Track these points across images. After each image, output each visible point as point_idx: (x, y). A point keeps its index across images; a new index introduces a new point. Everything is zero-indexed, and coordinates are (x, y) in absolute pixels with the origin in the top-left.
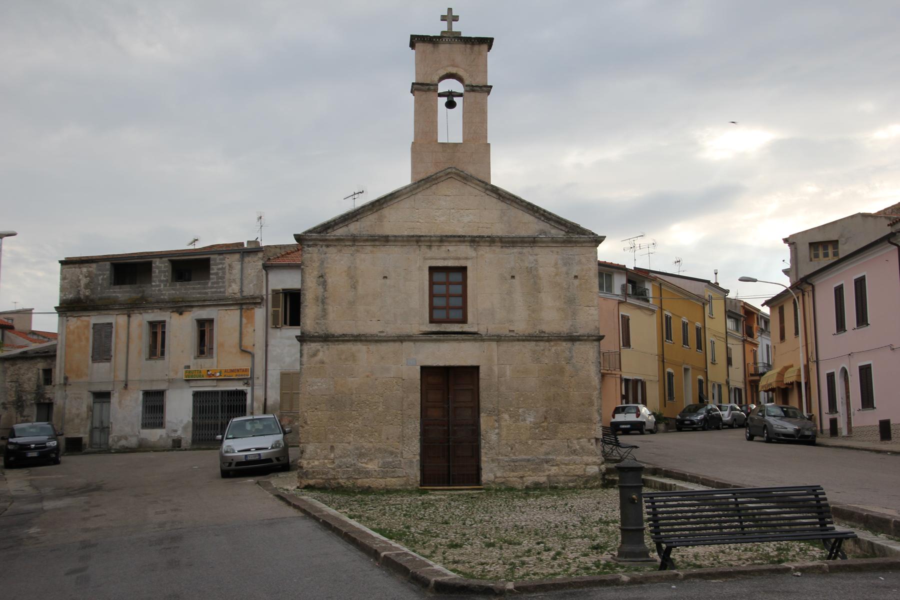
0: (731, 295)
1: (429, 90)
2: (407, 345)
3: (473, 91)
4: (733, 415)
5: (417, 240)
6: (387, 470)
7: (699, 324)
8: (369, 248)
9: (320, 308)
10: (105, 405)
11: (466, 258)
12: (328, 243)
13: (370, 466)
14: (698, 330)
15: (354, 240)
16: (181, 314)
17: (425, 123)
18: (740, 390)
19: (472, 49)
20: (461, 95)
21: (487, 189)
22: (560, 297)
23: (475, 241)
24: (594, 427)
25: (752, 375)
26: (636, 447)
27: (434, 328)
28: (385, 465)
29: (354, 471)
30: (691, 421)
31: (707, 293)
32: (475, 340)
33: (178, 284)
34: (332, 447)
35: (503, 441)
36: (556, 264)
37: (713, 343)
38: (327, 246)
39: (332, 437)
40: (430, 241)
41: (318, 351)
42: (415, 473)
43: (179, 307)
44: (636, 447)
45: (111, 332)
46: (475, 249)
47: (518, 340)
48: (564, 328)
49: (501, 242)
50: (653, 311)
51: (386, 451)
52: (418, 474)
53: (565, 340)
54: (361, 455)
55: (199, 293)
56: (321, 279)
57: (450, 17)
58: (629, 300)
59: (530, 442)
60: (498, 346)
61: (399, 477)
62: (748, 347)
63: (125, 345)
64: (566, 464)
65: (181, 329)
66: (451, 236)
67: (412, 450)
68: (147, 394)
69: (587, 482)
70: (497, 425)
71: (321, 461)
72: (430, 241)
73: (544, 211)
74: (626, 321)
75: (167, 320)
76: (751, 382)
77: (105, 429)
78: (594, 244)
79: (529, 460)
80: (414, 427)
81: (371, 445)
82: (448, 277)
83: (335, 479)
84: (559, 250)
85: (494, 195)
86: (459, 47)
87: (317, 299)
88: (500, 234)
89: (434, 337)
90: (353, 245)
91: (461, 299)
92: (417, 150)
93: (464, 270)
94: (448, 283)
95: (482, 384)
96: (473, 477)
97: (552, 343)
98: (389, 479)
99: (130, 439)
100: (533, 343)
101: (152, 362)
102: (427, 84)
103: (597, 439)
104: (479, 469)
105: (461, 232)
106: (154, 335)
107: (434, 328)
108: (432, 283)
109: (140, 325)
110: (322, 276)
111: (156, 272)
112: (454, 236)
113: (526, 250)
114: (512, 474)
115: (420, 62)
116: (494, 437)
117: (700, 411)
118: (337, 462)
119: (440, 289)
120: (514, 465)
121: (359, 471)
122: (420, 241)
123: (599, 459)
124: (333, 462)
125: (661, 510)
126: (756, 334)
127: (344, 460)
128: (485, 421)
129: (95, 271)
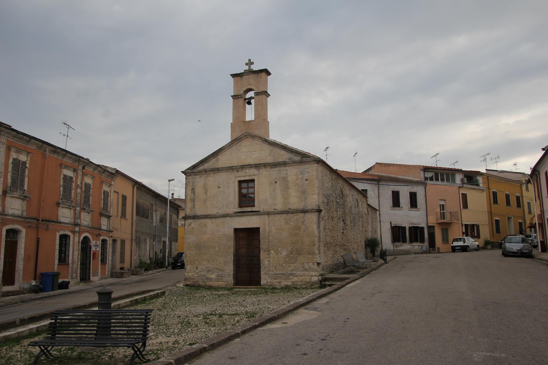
1: (238, 98)
3: (258, 95)
6: (220, 278)
11: (254, 175)
14: (518, 198)
15: (205, 171)
17: (239, 114)
19: (257, 76)
23: (257, 166)
32: (257, 215)
38: (196, 175)
42: (230, 280)
46: (258, 171)
47: (278, 214)
48: (300, 206)
50: (483, 190)
53: (301, 212)
54: (209, 271)
57: (250, 63)
58: (465, 186)
67: (230, 269)
69: (312, 285)
74: (464, 196)
79: (283, 274)
80: (231, 258)
82: (248, 185)
86: (252, 76)
87: (191, 200)
89: (239, 214)
95: (261, 236)
100: (285, 215)
110: (193, 189)
113: (281, 169)
115: (236, 85)
116: (266, 262)
119: (251, 190)
125: (113, 321)
127: (201, 273)
128: (263, 255)
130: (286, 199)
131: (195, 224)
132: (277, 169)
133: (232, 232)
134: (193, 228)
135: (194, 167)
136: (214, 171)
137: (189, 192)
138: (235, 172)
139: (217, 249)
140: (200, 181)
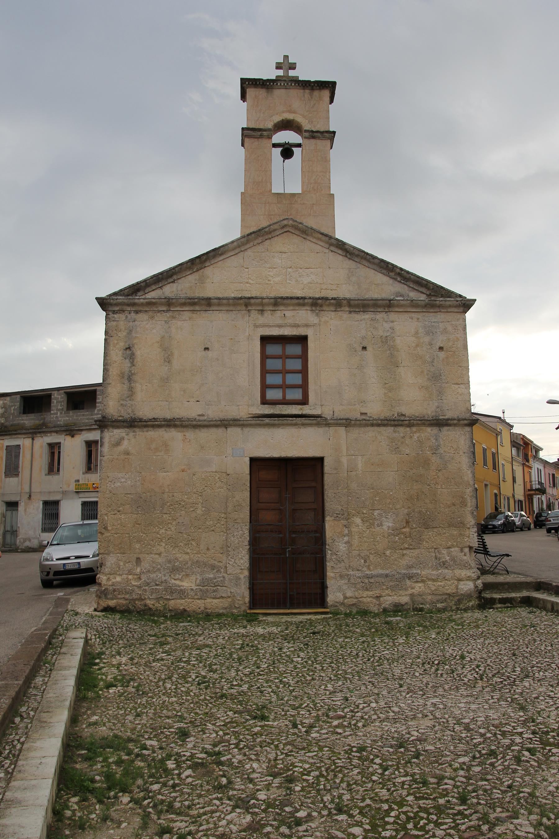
0: (514, 430)
1: (261, 136)
2: (233, 431)
3: (313, 137)
4: (523, 520)
5: (245, 303)
6: (207, 588)
7: (494, 450)
8: (187, 315)
9: (126, 387)
10: (14, 512)
11: (307, 326)
12: (138, 308)
13: (186, 584)
14: (493, 454)
15: (169, 303)
16: (73, 436)
18: (521, 502)
19: (311, 95)
20: (299, 145)
21: (331, 245)
22: (422, 372)
23: (316, 304)
24: (467, 532)
25: (529, 490)
26: (508, 555)
27: (267, 410)
28: (204, 583)
29: (166, 590)
30: (493, 525)
31: (499, 427)
32: (318, 425)
33: (71, 413)
34: (138, 559)
35: (355, 555)
36: (417, 333)
37: (503, 465)
38: (137, 312)
39: (137, 546)
40: (262, 305)
41: (123, 438)
42: (242, 593)
43: (71, 431)
44: (508, 555)
45: (19, 453)
46: (317, 315)
47: (372, 425)
48: (428, 410)
49: (350, 305)
51: (205, 564)
52: (247, 593)
54: (174, 570)
55: (88, 419)
56: (128, 352)
57: (286, 64)
59: (388, 553)
60: (347, 432)
61: (222, 597)
62: (526, 469)
63: (30, 463)
64: (434, 580)
65: (73, 449)
66: (287, 298)
68: (46, 503)
69: (459, 601)
70: (346, 531)
71: (125, 576)
72: (262, 305)
73: (401, 269)
75: (62, 442)
76: (529, 495)
77: (14, 532)
78: (461, 309)
79: (387, 576)
80: (241, 535)
81: (187, 557)
82: (284, 350)
83: (141, 599)
84: (419, 316)
85: (340, 252)
86: (296, 93)
87: (122, 375)
88: (348, 296)
89: (267, 420)
90: (167, 311)
91: (300, 376)
92: (247, 202)
93: (303, 340)
94: (284, 357)
95: (327, 479)
96: (317, 598)
97: (414, 429)
98: (209, 600)
99: (32, 541)
100: (391, 429)
101: (50, 477)
102: (260, 130)
103: (470, 548)
104: (323, 587)
105: (299, 294)
106: (52, 454)
107: (267, 410)
108: (264, 357)
109: (42, 447)
110: (129, 348)
111: (54, 402)
112: (292, 298)
113: (379, 316)
114: (366, 593)
117: (498, 517)
118: (144, 578)
120: (368, 583)
121: (172, 590)
122: (250, 304)
123: (473, 573)
124: (140, 578)
126: (531, 460)
128: (331, 527)
129: (8, 403)
130: (390, 390)
131: (132, 441)
132: (367, 316)
134: (127, 453)
135: (136, 289)
136: (194, 304)
137: (117, 355)
138: (254, 314)
139: (199, 512)
140: (149, 330)
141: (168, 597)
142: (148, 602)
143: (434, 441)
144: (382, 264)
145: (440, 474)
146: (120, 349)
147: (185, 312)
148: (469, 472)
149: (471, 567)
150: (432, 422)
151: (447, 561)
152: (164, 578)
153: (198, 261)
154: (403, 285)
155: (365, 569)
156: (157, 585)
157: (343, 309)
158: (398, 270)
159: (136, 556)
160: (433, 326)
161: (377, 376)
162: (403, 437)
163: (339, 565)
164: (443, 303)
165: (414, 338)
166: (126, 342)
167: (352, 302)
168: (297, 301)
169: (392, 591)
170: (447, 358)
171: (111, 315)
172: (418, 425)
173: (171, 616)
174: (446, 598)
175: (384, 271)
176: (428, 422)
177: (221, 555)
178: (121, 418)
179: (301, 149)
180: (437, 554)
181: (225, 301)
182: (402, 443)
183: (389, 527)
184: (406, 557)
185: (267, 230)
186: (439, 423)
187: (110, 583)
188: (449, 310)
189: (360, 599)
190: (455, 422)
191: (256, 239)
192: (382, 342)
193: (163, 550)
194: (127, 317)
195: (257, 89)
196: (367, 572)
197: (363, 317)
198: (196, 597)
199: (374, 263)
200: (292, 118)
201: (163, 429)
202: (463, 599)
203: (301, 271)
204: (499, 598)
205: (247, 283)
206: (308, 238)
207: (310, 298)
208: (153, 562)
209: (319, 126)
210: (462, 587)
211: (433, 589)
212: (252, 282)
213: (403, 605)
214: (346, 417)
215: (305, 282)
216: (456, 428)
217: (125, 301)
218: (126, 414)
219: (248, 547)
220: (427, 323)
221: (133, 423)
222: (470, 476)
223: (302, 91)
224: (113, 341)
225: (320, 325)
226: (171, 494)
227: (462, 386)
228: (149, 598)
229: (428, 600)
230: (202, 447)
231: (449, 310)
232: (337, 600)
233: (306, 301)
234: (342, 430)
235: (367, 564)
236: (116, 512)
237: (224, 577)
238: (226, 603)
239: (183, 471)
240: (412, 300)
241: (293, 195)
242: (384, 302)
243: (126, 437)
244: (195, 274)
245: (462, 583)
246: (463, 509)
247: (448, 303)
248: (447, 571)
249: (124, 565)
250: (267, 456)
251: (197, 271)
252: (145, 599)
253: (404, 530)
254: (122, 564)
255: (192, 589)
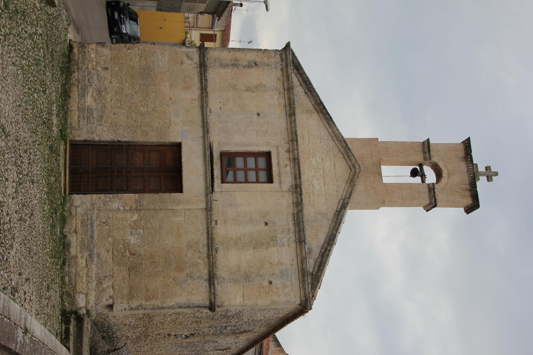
1: (424, 153)
3: (430, 190)
6: (86, 113)
8: (283, 102)
11: (280, 183)
12: (284, 70)
15: (289, 89)
19: (466, 190)
20: (423, 181)
23: (297, 189)
24: (125, 302)
27: (216, 155)
28: (90, 110)
29: (85, 85)
32: (207, 188)
34: (107, 69)
36: (281, 264)
38: (282, 70)
39: (117, 68)
41: (192, 60)
42: (82, 135)
47: (208, 228)
48: (221, 271)
49: (298, 212)
52: (82, 138)
54: (99, 92)
57: (490, 175)
59: (110, 239)
61: (79, 122)
64: (87, 274)
66: (299, 167)
69: (69, 295)
79: (92, 237)
80: (125, 135)
81: (109, 100)
82: (262, 170)
84: (295, 266)
85: (339, 207)
86: (466, 179)
87: (236, 60)
89: (208, 153)
90: (284, 89)
95: (166, 196)
97: (206, 260)
98: (77, 113)
100: (205, 242)
102: (429, 151)
110: (256, 64)
112: (299, 169)
114: (79, 222)
118: (94, 72)
120: (88, 223)
124: (93, 69)
128: (130, 198)
130: (236, 243)
132: (291, 226)
133: (174, 138)
134: (182, 63)
135: (298, 67)
137: (251, 57)
138: (286, 146)
139: (141, 109)
140: (271, 77)
141: (80, 87)
142: (76, 74)
143: (197, 275)
144: (333, 237)
145: (171, 280)
146: (254, 59)
147: (284, 100)
148: (173, 303)
149: (97, 305)
150: (212, 273)
151: (102, 284)
152: (93, 84)
153: (322, 107)
154: (318, 254)
155: (98, 222)
156: (88, 80)
157: (295, 208)
158: (329, 248)
159: (109, 67)
160: (288, 276)
161: (245, 233)
162: (199, 252)
163: (101, 203)
164: (307, 283)
165: (277, 261)
166: (260, 62)
167: (300, 213)
168: (297, 174)
169: (80, 242)
170: (263, 287)
171: (279, 53)
172: (209, 262)
173: (66, 88)
174: (72, 284)
175: (328, 239)
176: (211, 269)
177: (110, 123)
178: (206, 59)
179: (421, 182)
180: (108, 278)
181: (293, 125)
182: (195, 251)
183: (130, 240)
184: (106, 253)
185: (350, 154)
186: (211, 279)
187: (90, 50)
188: (302, 289)
189: (74, 218)
190: (213, 291)
191: (343, 147)
192: (272, 237)
193: (114, 85)
194: (278, 63)
195: (463, 150)
196: (95, 224)
197: (290, 224)
198: (79, 105)
199: (333, 231)
200: (443, 175)
201: (200, 86)
202: (71, 298)
203: (322, 179)
204: (70, 328)
205: (309, 142)
206: (348, 184)
207: (300, 182)
208: (105, 78)
209: (440, 195)
210: (81, 297)
211: (80, 273)
212: (310, 145)
213: (68, 250)
214: (213, 207)
215: (313, 182)
216: (208, 293)
217: (289, 61)
218: (209, 62)
219: (116, 140)
220: (290, 272)
221: (203, 66)
222: (171, 304)
223: (468, 183)
224: (260, 54)
225: (282, 191)
226: (153, 90)
227: (242, 299)
228: (79, 74)
229: (71, 269)
230: (187, 111)
231: (302, 289)
232: (74, 201)
233: (298, 180)
234: (203, 206)
235: (102, 224)
236: (140, 55)
237: (94, 123)
238: (75, 124)
239: (171, 99)
240: (306, 258)
241: (380, 174)
242: (303, 237)
243: (193, 62)
244: (313, 107)
245: (84, 297)
246: (144, 298)
247: (307, 286)
248: (95, 284)
249: (103, 60)
250: (182, 154)
251: (315, 109)
252: (78, 72)
253: (128, 252)
254: (104, 58)
255: (85, 102)
